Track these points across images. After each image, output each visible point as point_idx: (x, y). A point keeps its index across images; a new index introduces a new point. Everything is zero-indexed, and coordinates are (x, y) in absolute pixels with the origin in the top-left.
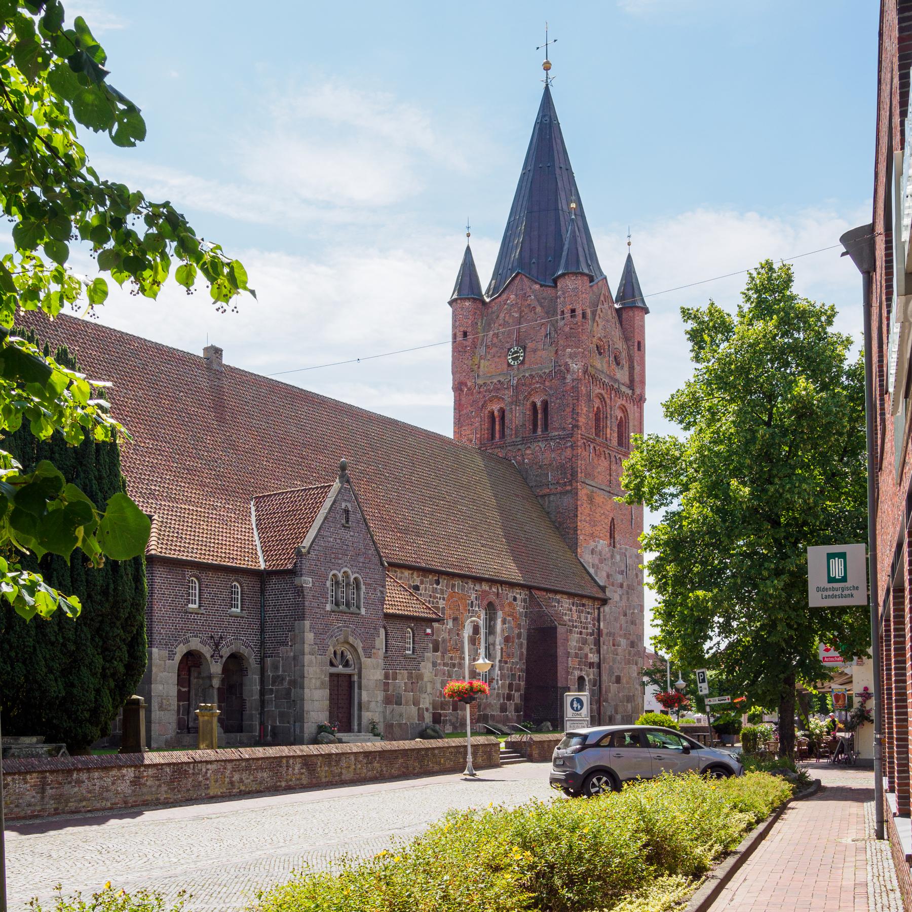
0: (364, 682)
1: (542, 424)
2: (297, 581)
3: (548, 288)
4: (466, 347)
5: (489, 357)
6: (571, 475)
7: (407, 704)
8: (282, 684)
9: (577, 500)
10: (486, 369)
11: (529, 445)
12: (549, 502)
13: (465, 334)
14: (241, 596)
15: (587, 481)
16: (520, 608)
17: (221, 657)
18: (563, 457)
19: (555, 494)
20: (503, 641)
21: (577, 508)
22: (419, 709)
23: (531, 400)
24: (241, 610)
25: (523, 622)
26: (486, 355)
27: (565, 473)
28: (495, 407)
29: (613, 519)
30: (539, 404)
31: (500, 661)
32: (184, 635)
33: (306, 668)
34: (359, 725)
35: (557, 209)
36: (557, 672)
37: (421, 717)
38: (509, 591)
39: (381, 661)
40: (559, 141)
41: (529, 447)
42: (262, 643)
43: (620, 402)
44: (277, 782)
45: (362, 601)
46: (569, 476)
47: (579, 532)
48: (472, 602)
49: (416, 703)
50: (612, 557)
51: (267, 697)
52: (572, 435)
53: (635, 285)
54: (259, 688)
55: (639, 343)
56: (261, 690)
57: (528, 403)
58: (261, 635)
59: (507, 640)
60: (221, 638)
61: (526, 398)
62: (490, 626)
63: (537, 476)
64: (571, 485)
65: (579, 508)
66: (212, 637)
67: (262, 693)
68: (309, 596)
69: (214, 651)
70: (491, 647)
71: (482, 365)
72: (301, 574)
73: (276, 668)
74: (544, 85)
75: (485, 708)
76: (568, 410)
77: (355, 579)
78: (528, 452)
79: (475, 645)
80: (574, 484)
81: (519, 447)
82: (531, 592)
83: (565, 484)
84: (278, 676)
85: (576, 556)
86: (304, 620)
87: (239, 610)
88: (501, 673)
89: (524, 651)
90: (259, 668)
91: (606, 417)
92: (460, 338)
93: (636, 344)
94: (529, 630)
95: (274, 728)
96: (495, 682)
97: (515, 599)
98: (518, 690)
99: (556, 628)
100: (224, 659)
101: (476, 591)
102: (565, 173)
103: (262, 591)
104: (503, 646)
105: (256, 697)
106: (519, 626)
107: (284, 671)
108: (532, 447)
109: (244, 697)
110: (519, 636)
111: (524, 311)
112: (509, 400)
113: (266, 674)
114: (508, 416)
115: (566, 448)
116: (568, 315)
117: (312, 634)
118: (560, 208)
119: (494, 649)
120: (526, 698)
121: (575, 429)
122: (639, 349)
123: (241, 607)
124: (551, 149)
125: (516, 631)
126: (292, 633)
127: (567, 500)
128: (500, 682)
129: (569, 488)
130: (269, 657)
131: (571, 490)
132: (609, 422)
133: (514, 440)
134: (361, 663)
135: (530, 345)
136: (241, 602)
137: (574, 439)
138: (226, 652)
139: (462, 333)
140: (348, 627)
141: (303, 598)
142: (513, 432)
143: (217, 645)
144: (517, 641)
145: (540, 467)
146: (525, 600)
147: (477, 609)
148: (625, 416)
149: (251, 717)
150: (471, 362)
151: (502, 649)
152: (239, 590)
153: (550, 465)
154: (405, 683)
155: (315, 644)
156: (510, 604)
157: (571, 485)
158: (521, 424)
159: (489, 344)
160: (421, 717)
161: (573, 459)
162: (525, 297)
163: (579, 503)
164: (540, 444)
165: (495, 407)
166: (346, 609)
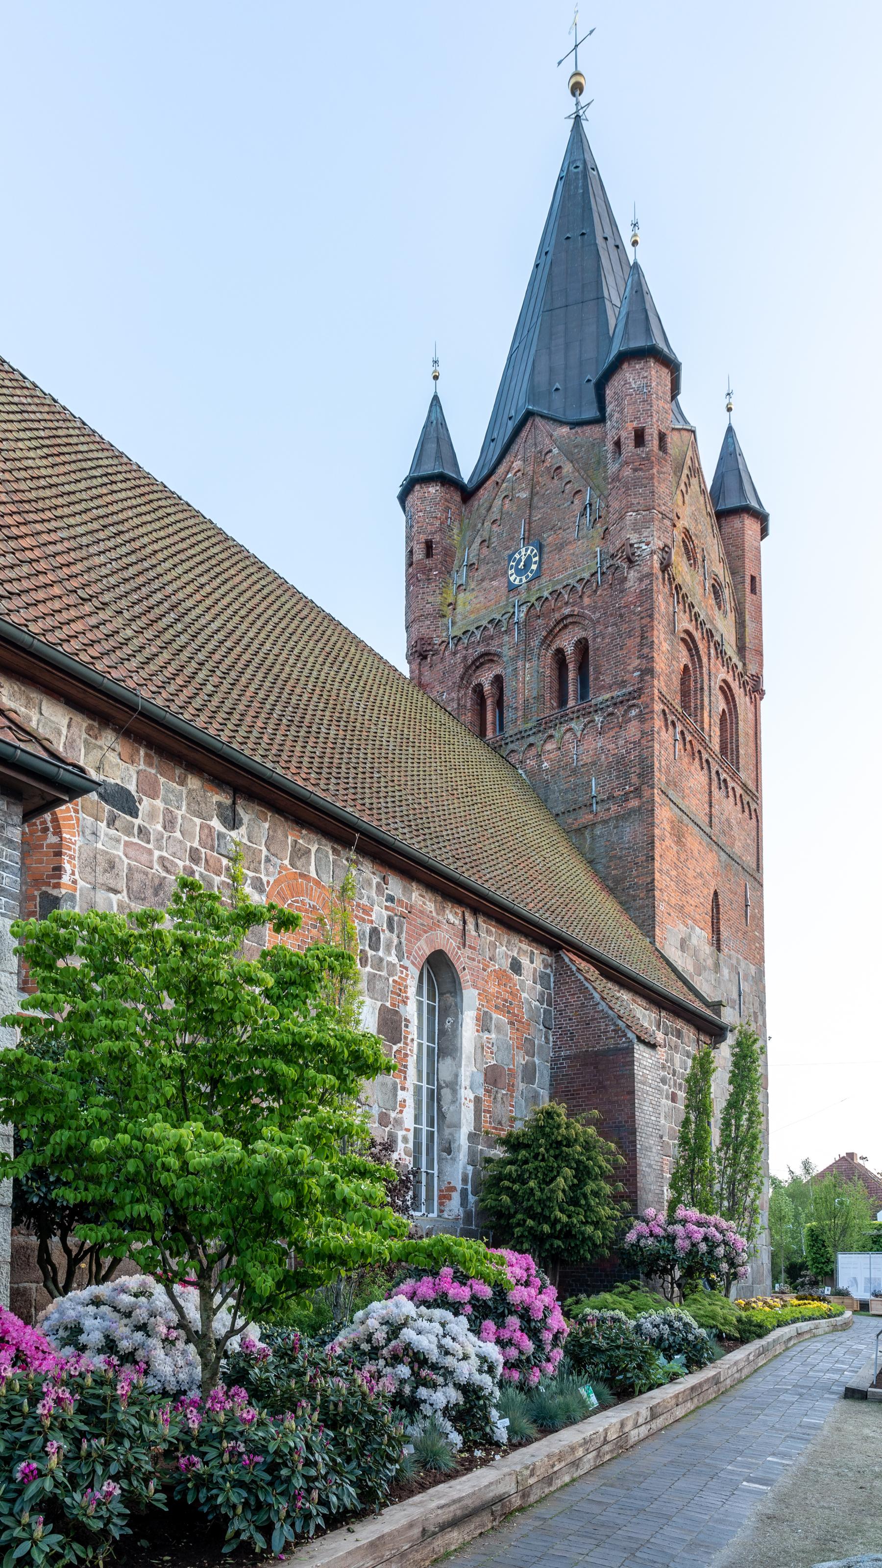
1: (575, 691)
3: (585, 428)
4: (431, 570)
5: (473, 585)
6: (640, 775)
9: (652, 825)
10: (468, 608)
11: (551, 732)
12: (593, 838)
15: (671, 793)
18: (621, 742)
19: (605, 822)
20: (480, 1078)
21: (653, 842)
23: (554, 647)
26: (467, 581)
27: (627, 775)
29: (716, 894)
30: (569, 650)
38: (498, 938)
41: (551, 736)
44: (129, 1437)
46: (634, 779)
47: (657, 893)
48: (375, 932)
50: (717, 966)
53: (743, 474)
55: (753, 578)
57: (550, 652)
62: (442, 1032)
63: (566, 791)
65: (657, 843)
70: (446, 1093)
71: (460, 602)
78: (549, 746)
80: (646, 794)
81: (531, 740)
82: (559, 959)
83: (626, 798)
85: (653, 943)
91: (702, 689)
92: (419, 555)
94: (554, 1061)
97: (516, 967)
101: (391, 899)
102: (613, 252)
104: (481, 1092)
106: (529, 1047)
108: (557, 735)
110: (529, 1073)
112: (512, 653)
115: (630, 720)
116: (629, 446)
118: (606, 295)
119: (455, 1100)
121: (648, 678)
122: (754, 590)
124: (587, 235)
125: (521, 1059)
127: (630, 831)
129: (634, 803)
131: (640, 807)
133: (521, 728)
135: (549, 539)
137: (644, 698)
139: (423, 546)
142: (520, 713)
144: (522, 1086)
145: (574, 771)
146: (543, 979)
147: (393, 959)
148: (730, 710)
150: (439, 599)
151: (477, 1100)
153: (594, 763)
158: (535, 694)
159: (474, 561)
162: (542, 456)
163: (657, 832)
164: (573, 725)
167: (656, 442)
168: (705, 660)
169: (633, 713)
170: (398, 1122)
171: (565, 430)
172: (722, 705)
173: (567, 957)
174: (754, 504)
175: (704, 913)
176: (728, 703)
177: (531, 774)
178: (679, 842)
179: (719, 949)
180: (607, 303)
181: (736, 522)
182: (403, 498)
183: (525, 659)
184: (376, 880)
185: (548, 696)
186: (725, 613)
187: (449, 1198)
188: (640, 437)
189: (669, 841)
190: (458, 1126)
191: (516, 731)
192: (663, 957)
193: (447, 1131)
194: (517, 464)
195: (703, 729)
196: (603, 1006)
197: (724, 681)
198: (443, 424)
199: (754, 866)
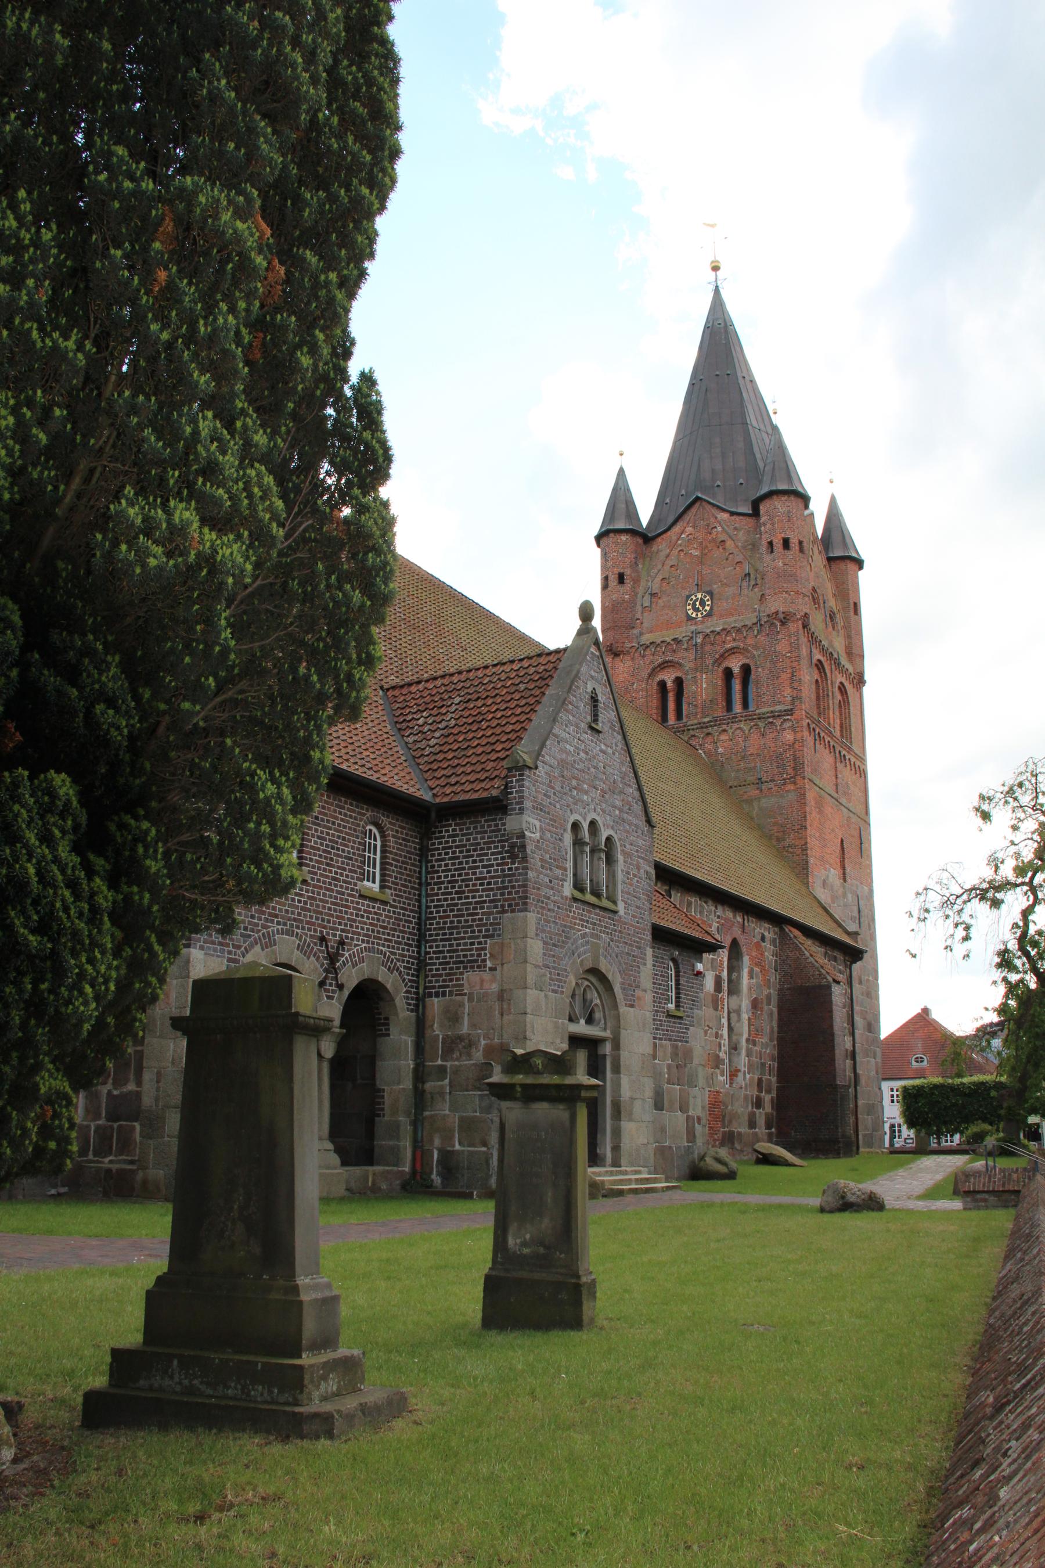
0: (624, 1054)
2: (511, 823)
6: (794, 769)
7: (671, 1110)
8: (469, 1056)
11: (724, 727)
13: (621, 579)
14: (382, 858)
16: (769, 951)
17: (341, 987)
22: (688, 1117)
24: (382, 887)
25: (773, 977)
28: (669, 677)
29: (842, 841)
30: (736, 670)
31: (748, 1040)
32: (264, 927)
33: (529, 1018)
34: (616, 1149)
35: (745, 423)
36: (834, 1060)
37: (691, 1136)
39: (649, 1016)
40: (738, 348)
41: (725, 731)
42: (421, 965)
43: (840, 678)
45: (620, 887)
49: (684, 1108)
51: (429, 1086)
52: (791, 712)
54: (411, 1064)
56: (416, 1070)
57: (721, 669)
58: (419, 947)
59: (755, 1005)
60: (342, 943)
61: (718, 662)
64: (795, 783)
66: (323, 939)
67: (420, 1075)
68: (535, 858)
69: (326, 971)
72: (521, 810)
73: (453, 1017)
74: (712, 287)
75: (730, 1122)
76: (785, 676)
77: (609, 839)
78: (723, 737)
79: (716, 1009)
82: (782, 930)
84: (461, 1038)
86: (526, 910)
87: (376, 887)
88: (749, 1061)
89: (775, 1024)
90: (413, 1020)
92: (613, 582)
93: (852, 606)
95: (447, 1156)
96: (740, 1075)
97: (763, 939)
98: (768, 1092)
99: (829, 987)
100: (346, 993)
101: (718, 917)
103: (423, 853)
105: (407, 1083)
107: (473, 1026)
109: (379, 1084)
111: (707, 547)
113: (428, 1033)
114: (689, 689)
115: (784, 729)
117: (540, 944)
119: (739, 1020)
120: (779, 1104)
123: (381, 881)
126: (496, 940)
128: (748, 1076)
130: (437, 995)
132: (831, 702)
134: (618, 1018)
136: (382, 869)
138: (351, 977)
140: (599, 938)
141: (525, 859)
142: (699, 710)
143: (333, 958)
149: (394, 1130)
151: (749, 1019)
152: (379, 843)
154: (669, 1066)
155: (547, 966)
156: (757, 945)
157: (795, 783)
160: (691, 1136)
161: (796, 746)
163: (808, 809)
165: (669, 677)
166: (592, 899)
167: (797, 548)
168: (828, 674)
169: (787, 725)
170: (722, 1036)
171: (726, 516)
172: (839, 697)
173: (787, 929)
174: (854, 555)
175: (835, 859)
176: (842, 695)
177: (709, 754)
178: (820, 812)
179: (845, 880)
180: (750, 428)
181: (842, 565)
182: (599, 538)
183: (701, 672)
184: (713, 908)
185: (720, 699)
186: (838, 632)
187: (736, 1076)
188: (786, 544)
189: (814, 814)
190: (741, 1035)
191: (696, 722)
192: (815, 897)
193: (734, 1038)
194: (689, 530)
195: (829, 724)
196: (811, 959)
197: (841, 683)
198: (628, 491)
199: (864, 811)
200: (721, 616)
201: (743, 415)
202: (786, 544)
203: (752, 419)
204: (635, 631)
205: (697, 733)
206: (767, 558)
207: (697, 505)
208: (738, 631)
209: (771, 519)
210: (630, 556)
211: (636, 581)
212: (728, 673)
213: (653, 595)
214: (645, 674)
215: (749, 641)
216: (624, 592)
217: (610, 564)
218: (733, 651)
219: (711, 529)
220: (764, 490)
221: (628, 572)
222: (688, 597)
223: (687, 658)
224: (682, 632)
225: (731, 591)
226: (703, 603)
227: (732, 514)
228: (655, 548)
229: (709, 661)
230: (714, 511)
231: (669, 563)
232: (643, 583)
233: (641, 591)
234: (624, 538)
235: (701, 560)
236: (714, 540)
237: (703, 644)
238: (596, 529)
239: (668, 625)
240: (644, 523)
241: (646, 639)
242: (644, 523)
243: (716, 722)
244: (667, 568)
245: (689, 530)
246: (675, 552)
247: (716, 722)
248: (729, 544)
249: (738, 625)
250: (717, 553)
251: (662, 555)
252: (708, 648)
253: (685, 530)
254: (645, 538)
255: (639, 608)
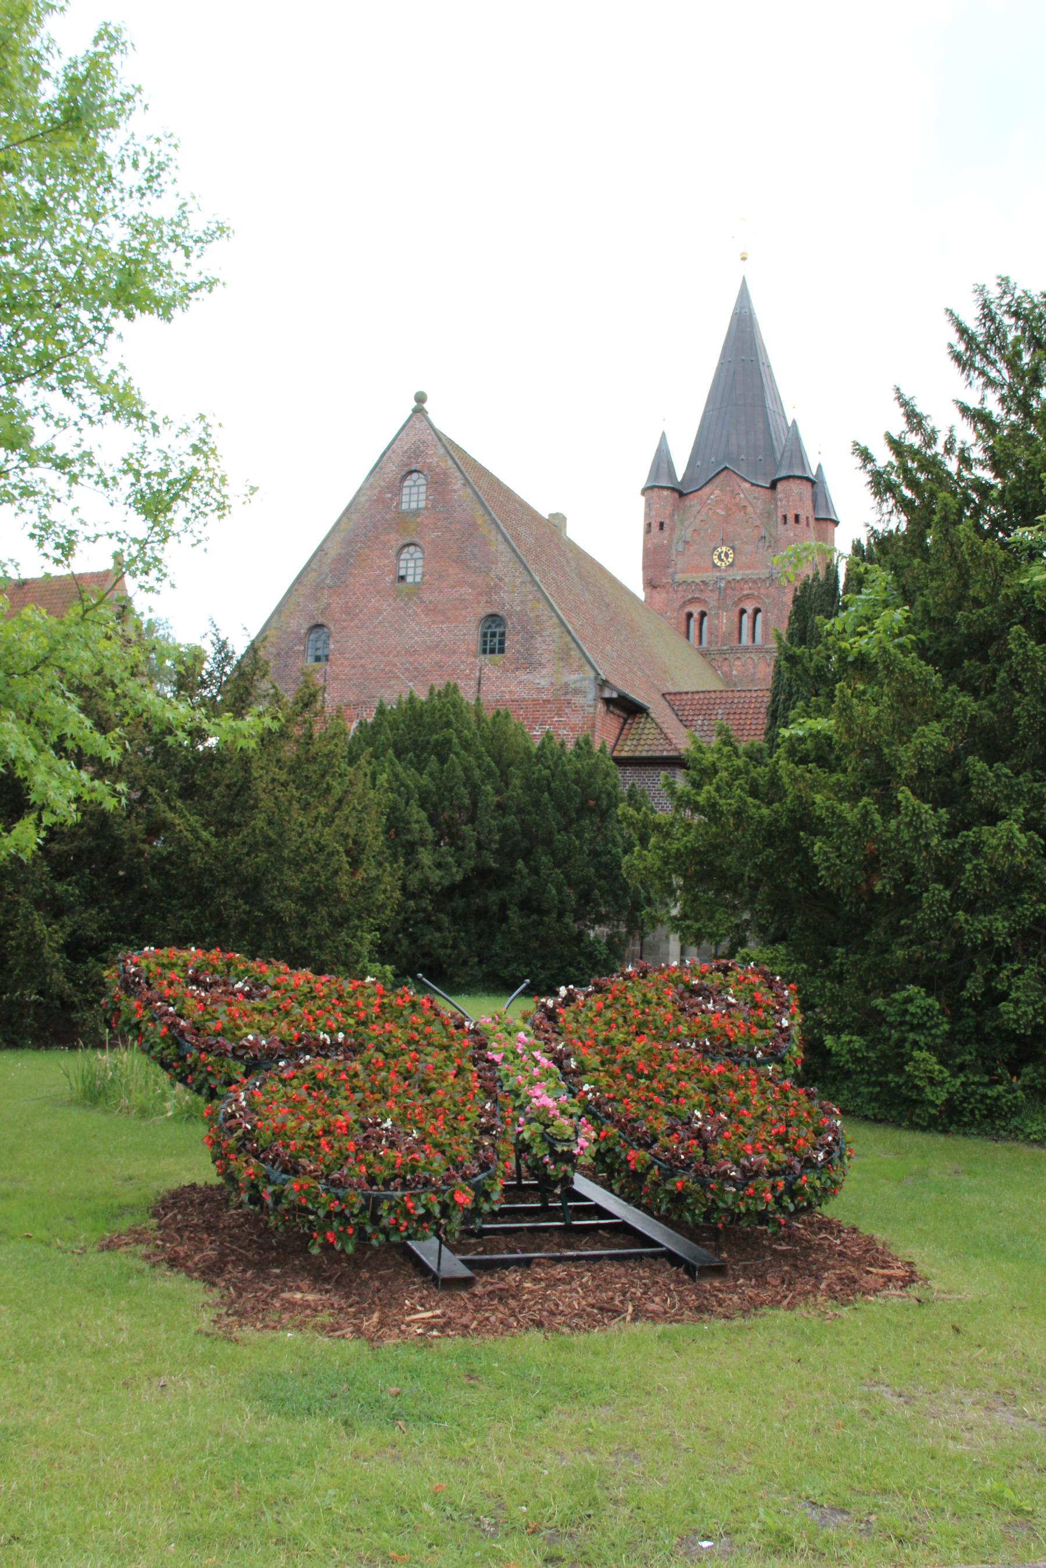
35: (764, 406)
61: (736, 604)
78: (737, 663)
171: (748, 485)
181: (824, 524)
182: (644, 491)
188: (797, 518)
194: (717, 492)
200: (741, 568)
201: (763, 399)
202: (797, 518)
203: (769, 403)
204: (670, 570)
205: (717, 657)
206: (781, 527)
207: (725, 473)
208: (755, 582)
209: (787, 497)
210: (670, 508)
211: (672, 529)
212: (690, 615)
213: (686, 542)
214: (677, 605)
215: (762, 591)
216: (663, 538)
217: (653, 513)
218: (748, 597)
219: (734, 495)
220: (783, 473)
221: (667, 522)
222: (715, 549)
223: (712, 599)
224: (709, 576)
225: (749, 548)
226: (727, 555)
227: (753, 485)
228: (687, 503)
229: (729, 602)
230: (738, 480)
231: (700, 517)
232: (677, 531)
233: (675, 538)
234: (665, 493)
235: (726, 519)
236: (736, 505)
237: (726, 588)
238: (642, 481)
239: (698, 569)
240: (679, 478)
241: (680, 577)
242: (679, 478)
243: (732, 650)
244: (698, 521)
245: (717, 492)
246: (705, 509)
247: (732, 650)
248: (750, 509)
249: (755, 577)
250: (739, 516)
251: (695, 510)
252: (729, 591)
253: (713, 493)
254: (680, 493)
255: (674, 552)
